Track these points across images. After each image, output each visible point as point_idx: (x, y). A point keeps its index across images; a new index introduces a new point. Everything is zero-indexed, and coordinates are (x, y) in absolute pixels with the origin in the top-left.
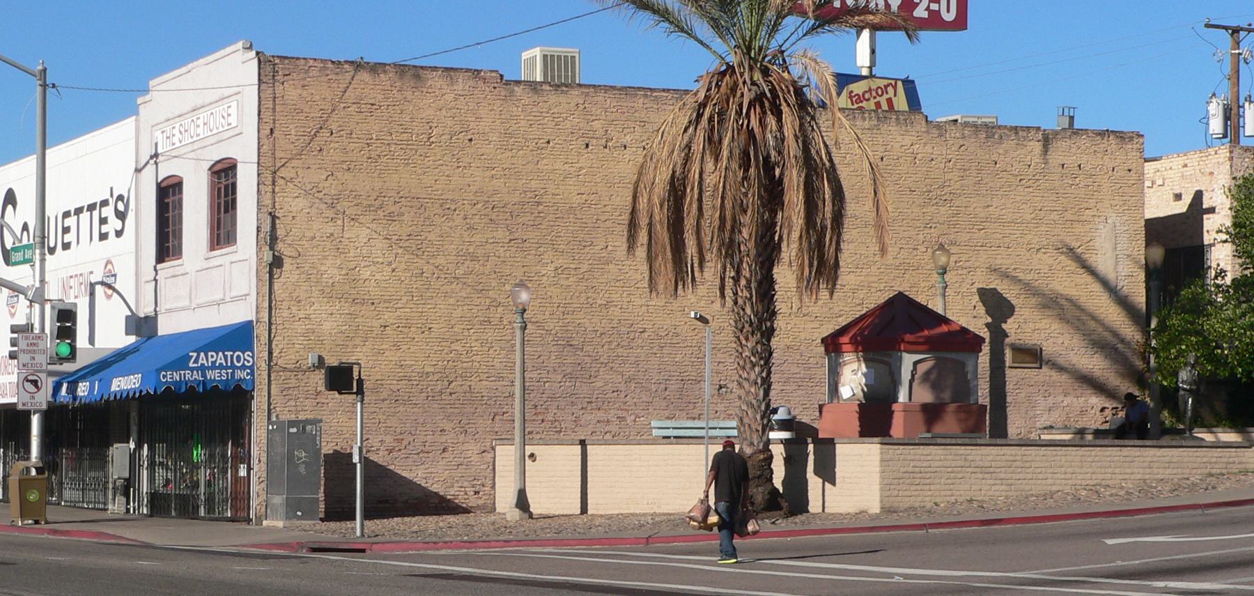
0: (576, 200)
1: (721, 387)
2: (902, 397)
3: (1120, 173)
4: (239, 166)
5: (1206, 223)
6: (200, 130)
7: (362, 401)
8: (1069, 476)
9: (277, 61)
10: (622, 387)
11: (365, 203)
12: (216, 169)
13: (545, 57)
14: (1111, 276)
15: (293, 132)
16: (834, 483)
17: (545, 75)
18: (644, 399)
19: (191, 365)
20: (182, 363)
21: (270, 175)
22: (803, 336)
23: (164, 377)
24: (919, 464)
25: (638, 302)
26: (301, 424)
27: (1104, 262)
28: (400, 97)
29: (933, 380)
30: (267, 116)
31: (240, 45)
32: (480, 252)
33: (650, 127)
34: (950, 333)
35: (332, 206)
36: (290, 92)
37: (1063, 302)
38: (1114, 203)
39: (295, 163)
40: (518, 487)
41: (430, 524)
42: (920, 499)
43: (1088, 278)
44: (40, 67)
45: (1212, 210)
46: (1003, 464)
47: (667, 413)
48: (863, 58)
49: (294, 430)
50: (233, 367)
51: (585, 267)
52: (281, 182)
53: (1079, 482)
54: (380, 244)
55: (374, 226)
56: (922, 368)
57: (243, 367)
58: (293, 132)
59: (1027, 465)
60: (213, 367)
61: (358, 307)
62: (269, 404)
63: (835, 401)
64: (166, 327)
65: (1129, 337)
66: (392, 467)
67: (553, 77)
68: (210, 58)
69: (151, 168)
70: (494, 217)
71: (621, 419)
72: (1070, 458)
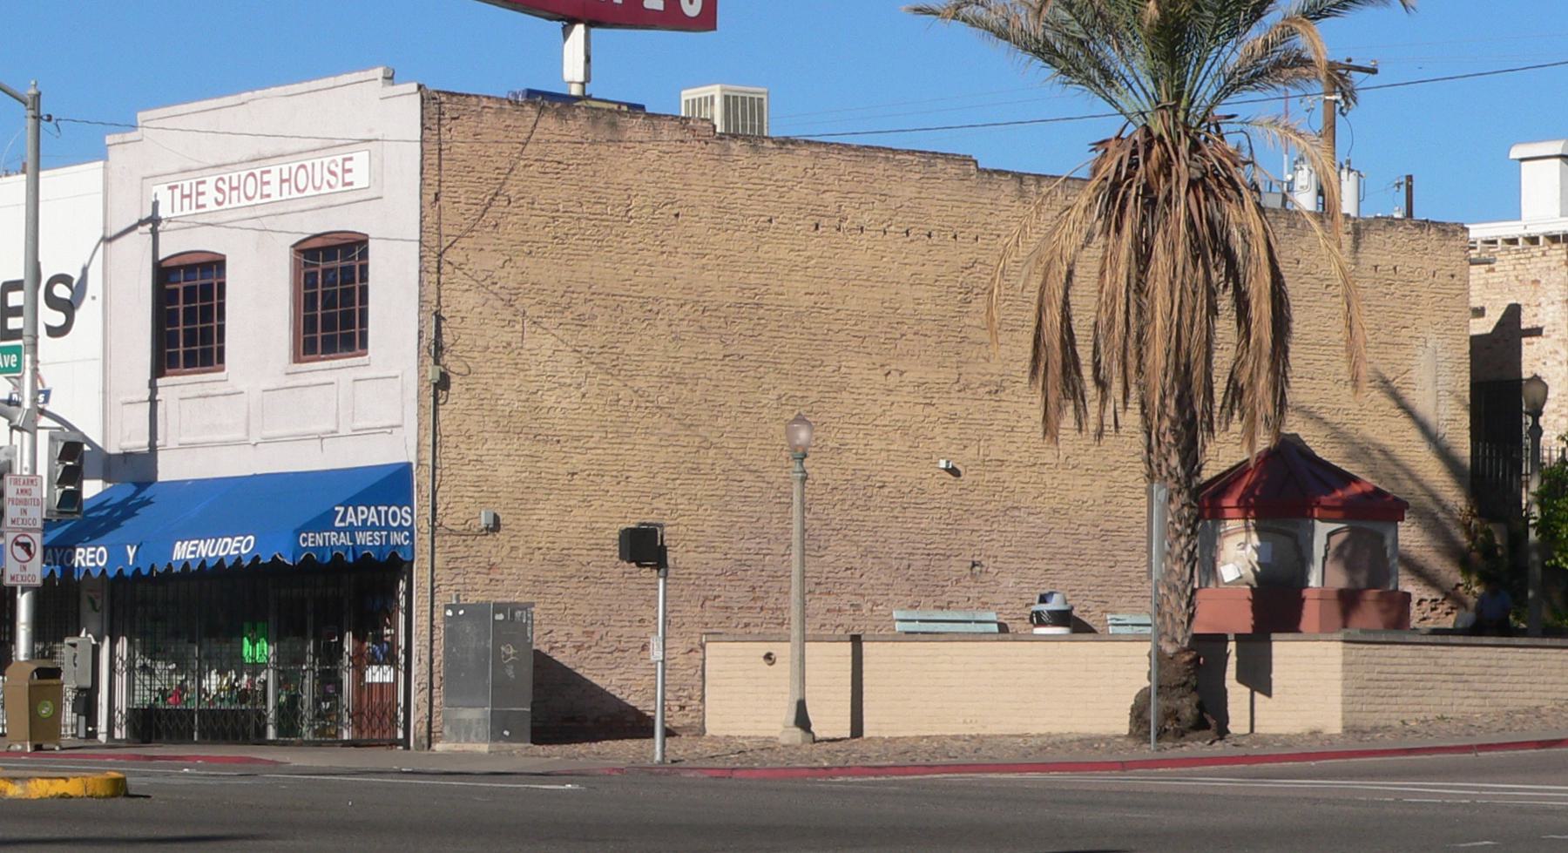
0: (807, 301)
1: (974, 565)
2: (1314, 580)
3: (1442, 279)
4: (372, 244)
5: (1525, 349)
6: (273, 190)
7: (665, 577)
8: (1548, 687)
9: (443, 99)
10: (857, 563)
11: (550, 300)
12: (306, 246)
13: (727, 98)
14: (1432, 420)
15: (462, 199)
16: (1268, 694)
17: (727, 125)
18: (884, 580)
19: (337, 524)
20: (324, 522)
21: (435, 258)
22: (1072, 495)
23: (305, 540)
24: (1386, 669)
25: (877, 445)
26: (508, 609)
27: (1423, 401)
28: (593, 153)
29: (1344, 555)
30: (432, 178)
31: (379, 72)
32: (688, 371)
33: (893, 203)
34: (1364, 494)
35: (509, 304)
36: (457, 136)
37: (1376, 454)
38: (1435, 320)
39: (465, 242)
40: (797, 698)
41: (622, 750)
42: (1385, 715)
43: (1405, 423)
44: (33, 91)
45: (1537, 332)
46: (1478, 670)
47: (910, 600)
48: (572, 69)
49: (500, 617)
50: (388, 528)
51: (814, 396)
52: (446, 268)
53: (1559, 695)
54: (568, 358)
55: (560, 333)
56: (1337, 540)
57: (401, 528)
58: (462, 199)
59: (1504, 671)
60: (364, 527)
61: (540, 447)
62: (433, 581)
63: (1212, 585)
64: (169, 469)
65: (1451, 504)
66: (580, 671)
67: (736, 126)
68: (297, 88)
69: (142, 237)
70: (705, 324)
71: (856, 607)
72: (1549, 664)
